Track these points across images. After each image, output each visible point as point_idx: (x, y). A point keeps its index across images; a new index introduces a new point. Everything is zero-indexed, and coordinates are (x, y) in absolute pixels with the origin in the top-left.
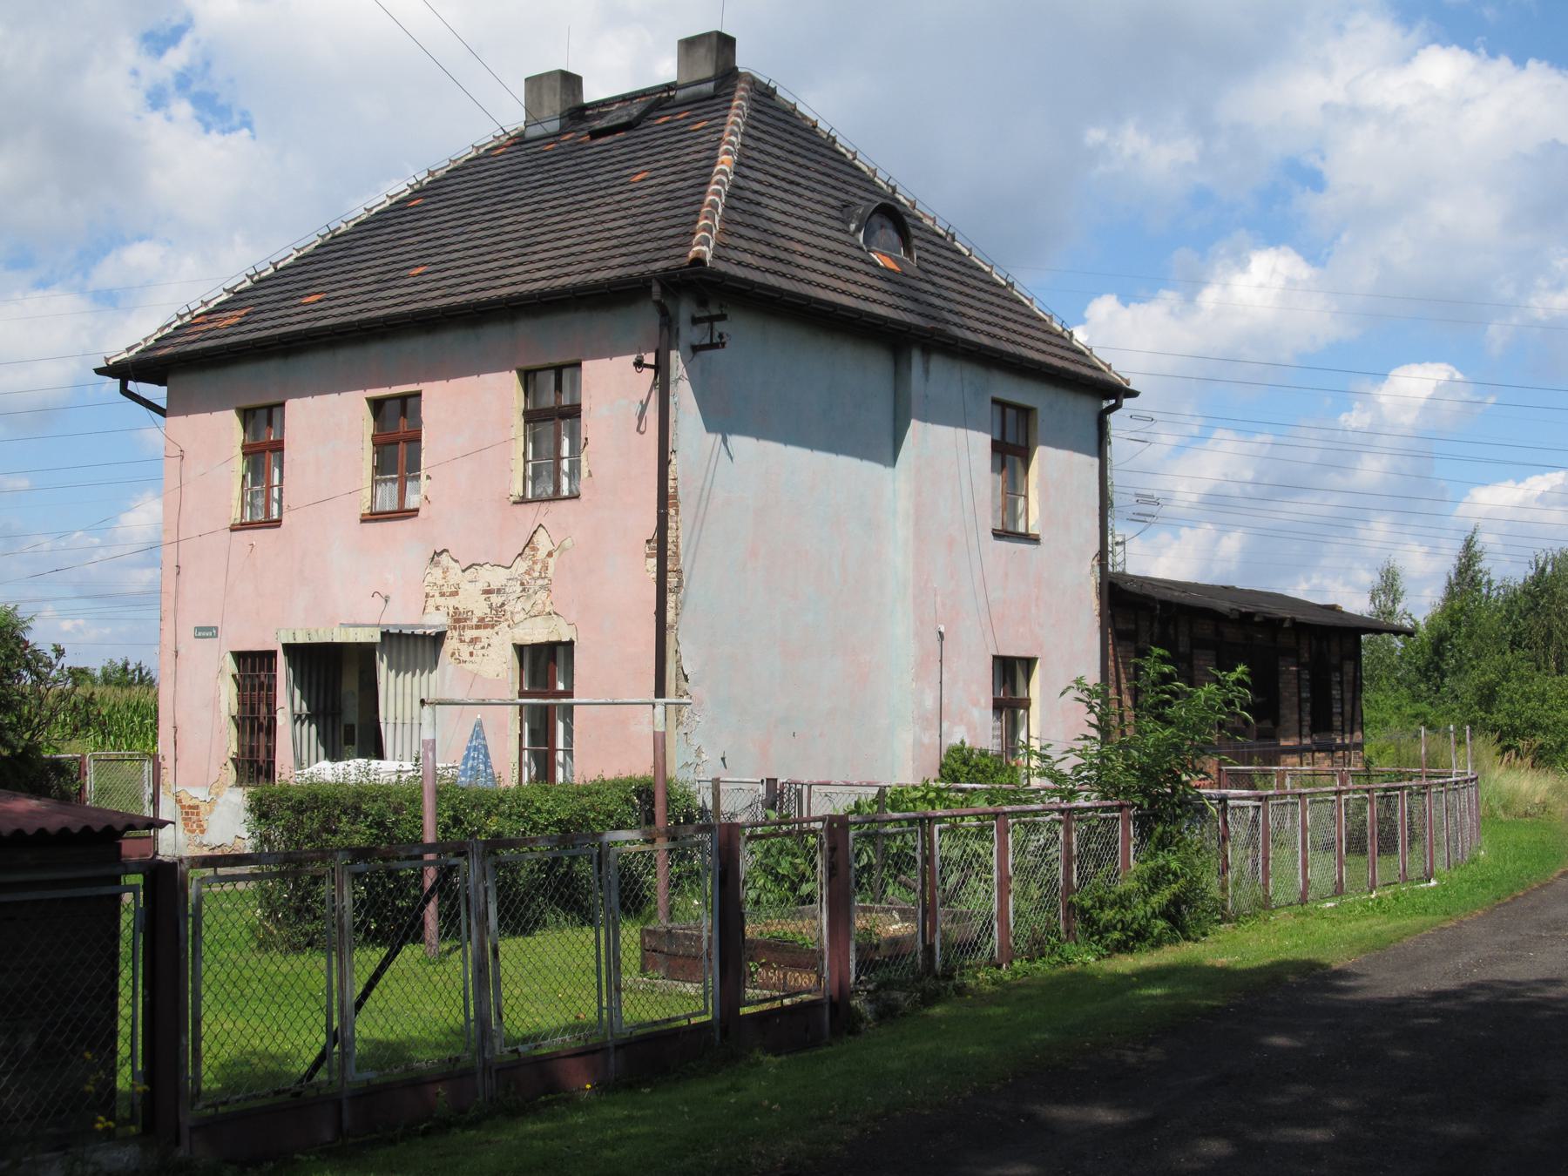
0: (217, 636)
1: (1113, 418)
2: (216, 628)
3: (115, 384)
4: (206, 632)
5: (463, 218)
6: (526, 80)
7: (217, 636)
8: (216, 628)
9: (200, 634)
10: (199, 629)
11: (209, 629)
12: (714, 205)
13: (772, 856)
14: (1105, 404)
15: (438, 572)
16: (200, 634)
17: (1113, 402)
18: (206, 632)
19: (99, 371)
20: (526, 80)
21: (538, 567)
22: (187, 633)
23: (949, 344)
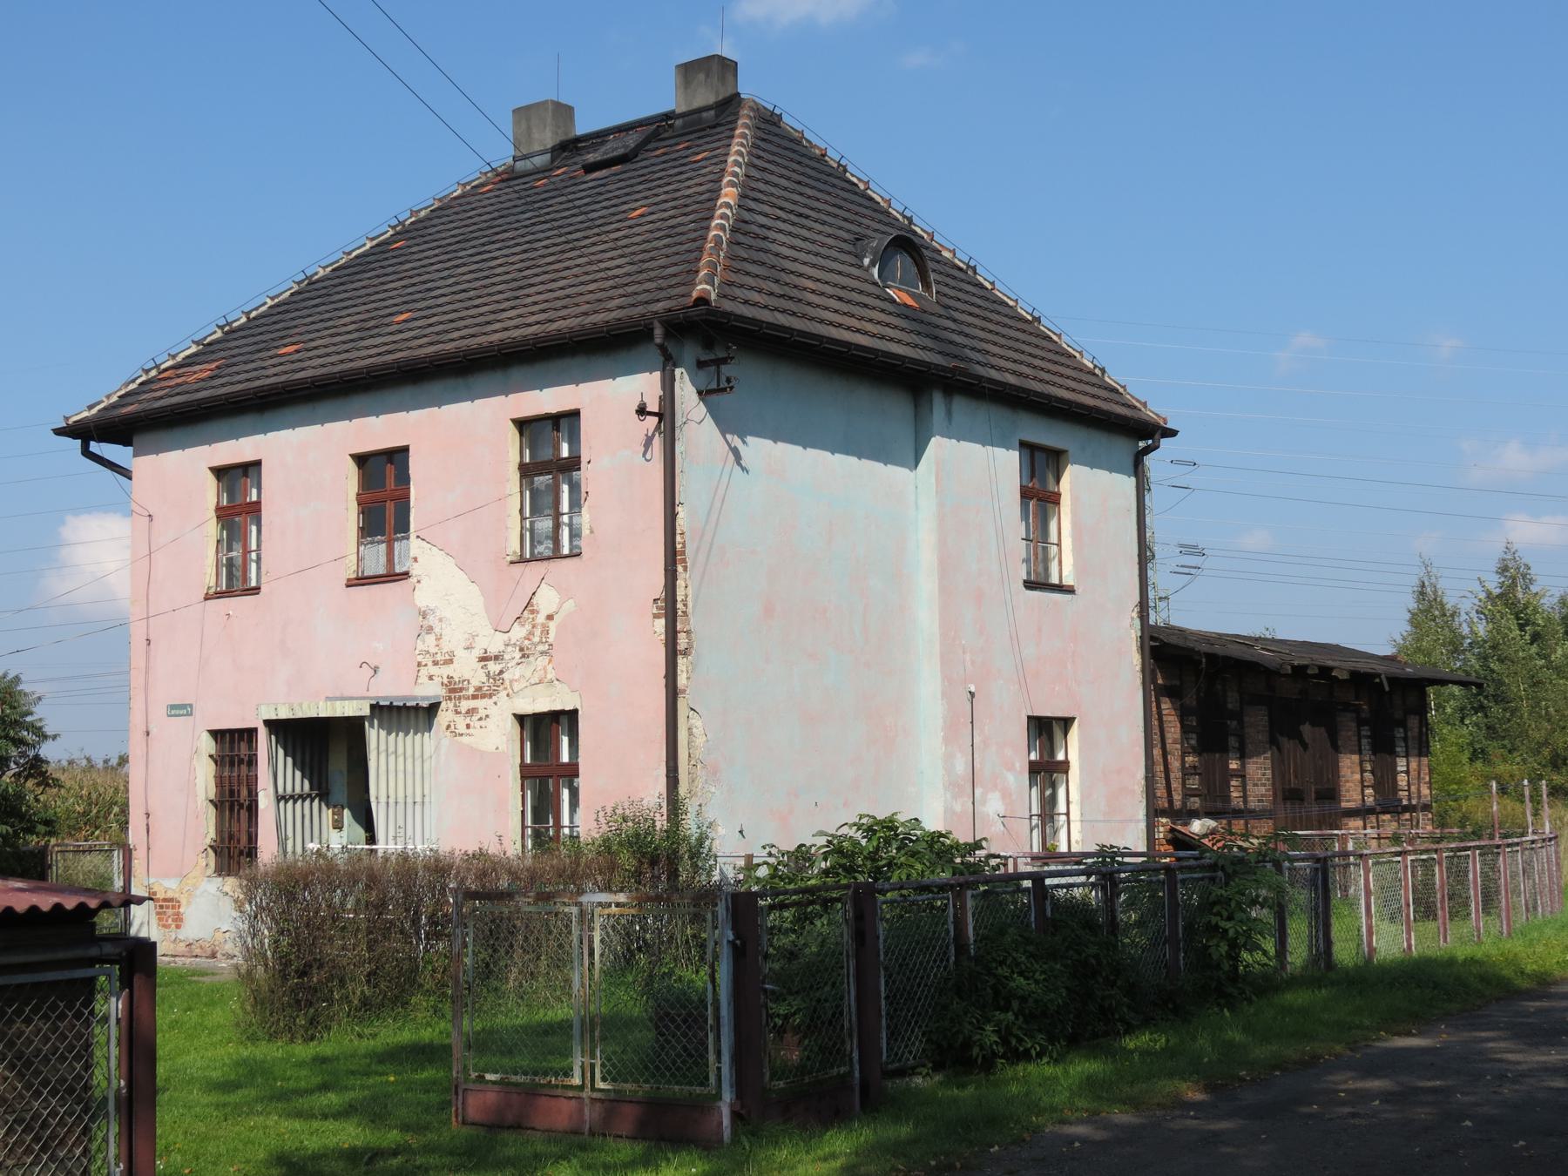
0: (191, 714)
2: (191, 706)
4: (181, 710)
7: (191, 714)
8: (191, 706)
9: (173, 712)
10: (173, 707)
16: (173, 712)
18: (181, 710)
21: (538, 632)
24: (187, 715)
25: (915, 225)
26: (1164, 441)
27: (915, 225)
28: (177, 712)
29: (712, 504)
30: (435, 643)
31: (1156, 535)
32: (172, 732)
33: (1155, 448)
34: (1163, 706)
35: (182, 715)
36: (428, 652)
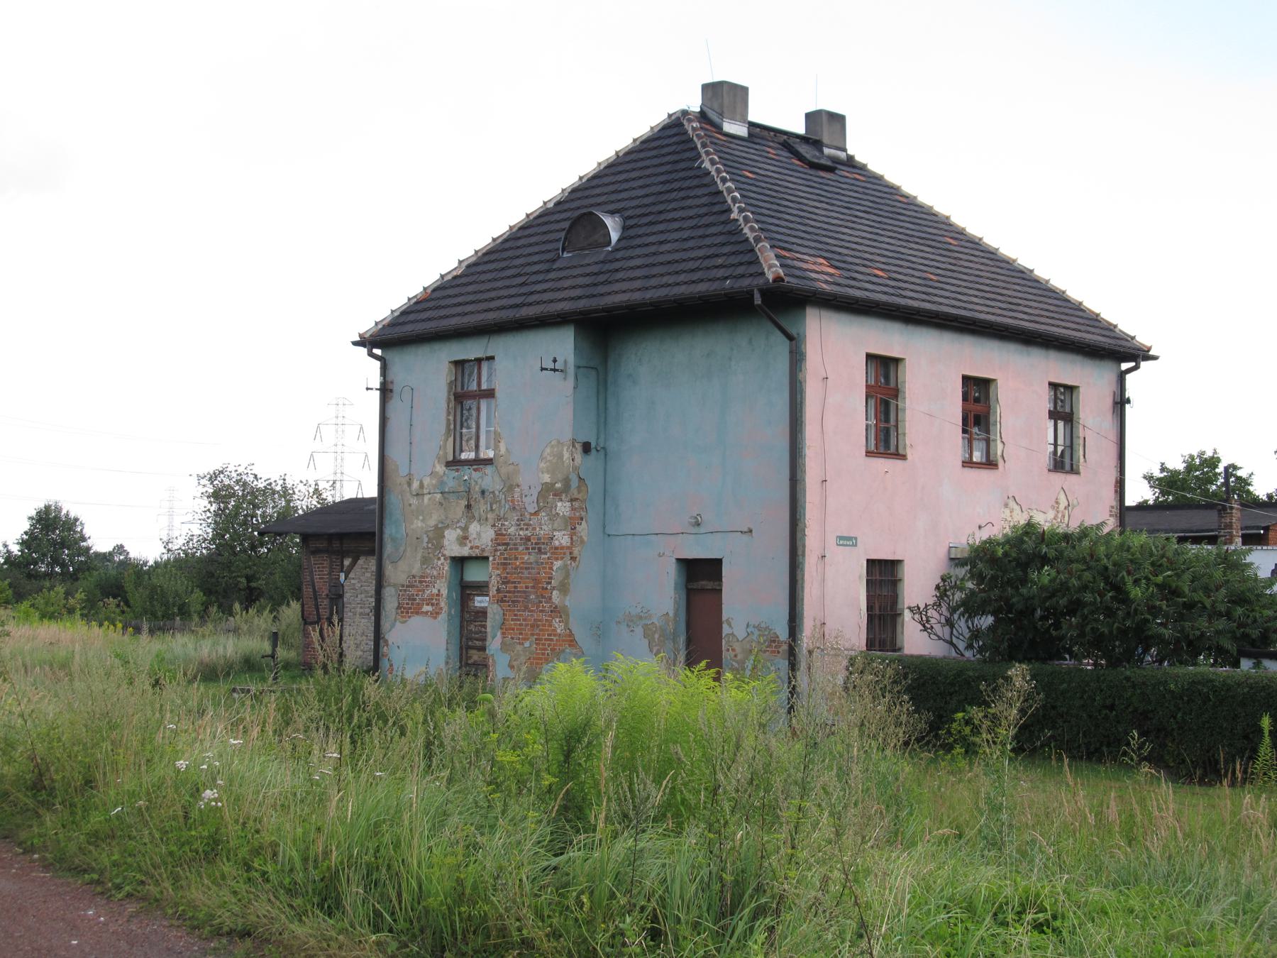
0: (856, 546)
1: (1129, 378)
2: (856, 538)
3: (363, 351)
4: (847, 541)
5: (920, 218)
6: (745, 90)
7: (856, 546)
8: (856, 538)
9: (841, 542)
10: (841, 538)
11: (849, 539)
12: (724, 180)
13: (796, 783)
14: (1125, 366)
15: (1007, 511)
16: (841, 542)
17: (1132, 364)
18: (847, 541)
19: (355, 343)
20: (745, 90)
21: (1060, 515)
22: (831, 540)
23: (829, 300)
24: (853, 545)
25: (490, 368)
26: (1143, 364)
27: (490, 368)
28: (845, 543)
29: (1072, 460)
30: (1009, 514)
31: (286, 482)
32: (838, 555)
33: (1136, 368)
34: (1059, 425)
35: (849, 545)
36: (1006, 520)
